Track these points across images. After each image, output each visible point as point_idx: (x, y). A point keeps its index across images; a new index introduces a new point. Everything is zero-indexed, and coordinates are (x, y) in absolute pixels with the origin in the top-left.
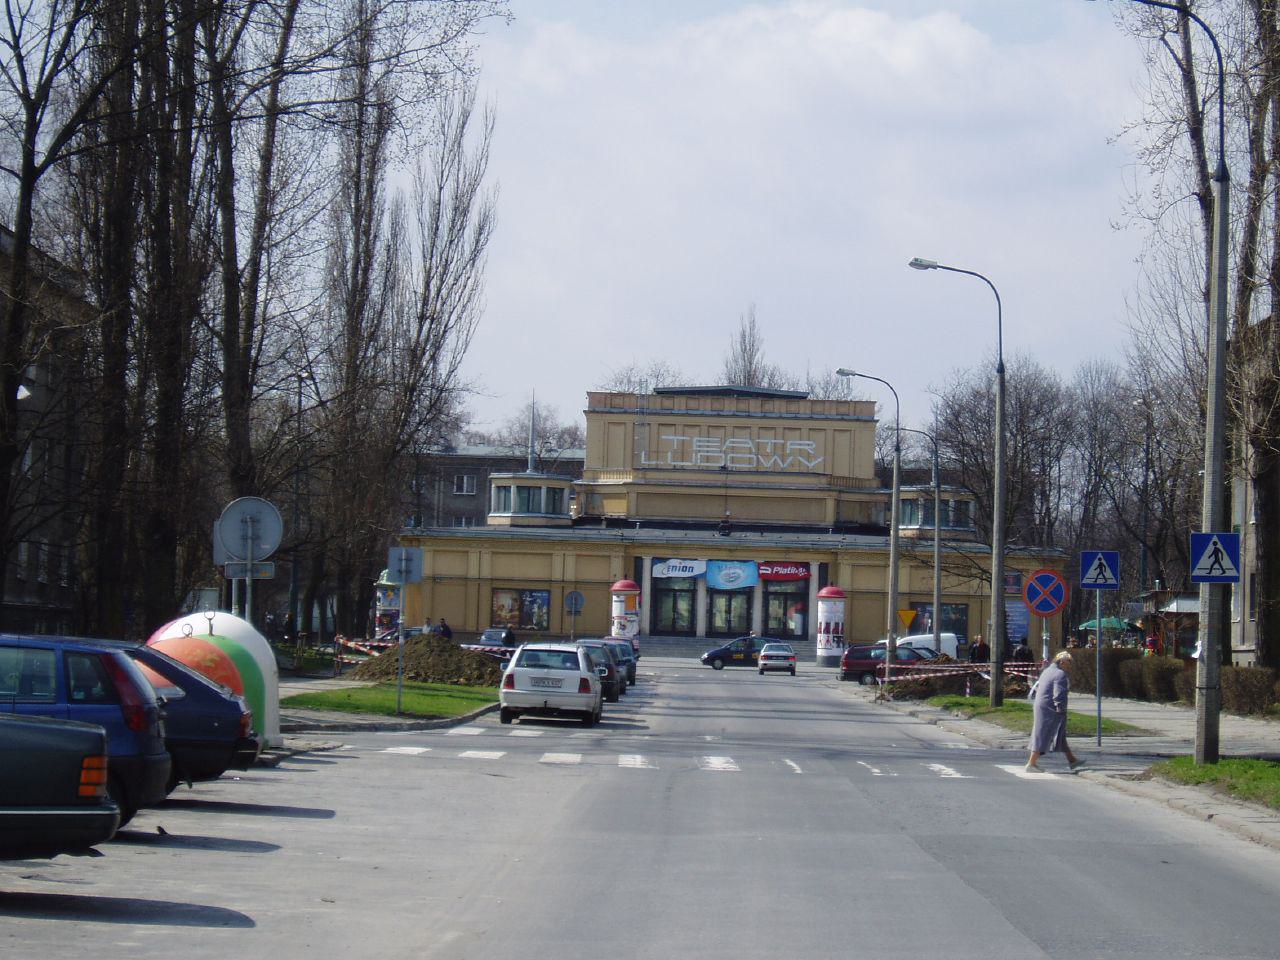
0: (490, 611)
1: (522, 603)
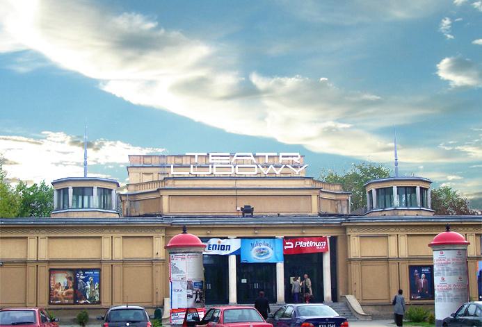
0: (47, 289)
1: (76, 281)
